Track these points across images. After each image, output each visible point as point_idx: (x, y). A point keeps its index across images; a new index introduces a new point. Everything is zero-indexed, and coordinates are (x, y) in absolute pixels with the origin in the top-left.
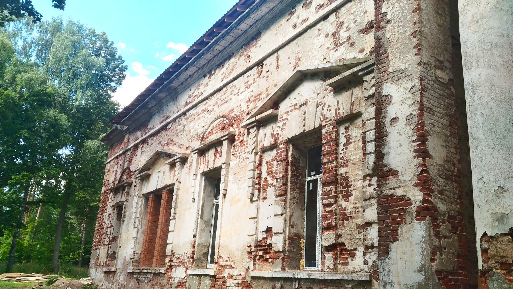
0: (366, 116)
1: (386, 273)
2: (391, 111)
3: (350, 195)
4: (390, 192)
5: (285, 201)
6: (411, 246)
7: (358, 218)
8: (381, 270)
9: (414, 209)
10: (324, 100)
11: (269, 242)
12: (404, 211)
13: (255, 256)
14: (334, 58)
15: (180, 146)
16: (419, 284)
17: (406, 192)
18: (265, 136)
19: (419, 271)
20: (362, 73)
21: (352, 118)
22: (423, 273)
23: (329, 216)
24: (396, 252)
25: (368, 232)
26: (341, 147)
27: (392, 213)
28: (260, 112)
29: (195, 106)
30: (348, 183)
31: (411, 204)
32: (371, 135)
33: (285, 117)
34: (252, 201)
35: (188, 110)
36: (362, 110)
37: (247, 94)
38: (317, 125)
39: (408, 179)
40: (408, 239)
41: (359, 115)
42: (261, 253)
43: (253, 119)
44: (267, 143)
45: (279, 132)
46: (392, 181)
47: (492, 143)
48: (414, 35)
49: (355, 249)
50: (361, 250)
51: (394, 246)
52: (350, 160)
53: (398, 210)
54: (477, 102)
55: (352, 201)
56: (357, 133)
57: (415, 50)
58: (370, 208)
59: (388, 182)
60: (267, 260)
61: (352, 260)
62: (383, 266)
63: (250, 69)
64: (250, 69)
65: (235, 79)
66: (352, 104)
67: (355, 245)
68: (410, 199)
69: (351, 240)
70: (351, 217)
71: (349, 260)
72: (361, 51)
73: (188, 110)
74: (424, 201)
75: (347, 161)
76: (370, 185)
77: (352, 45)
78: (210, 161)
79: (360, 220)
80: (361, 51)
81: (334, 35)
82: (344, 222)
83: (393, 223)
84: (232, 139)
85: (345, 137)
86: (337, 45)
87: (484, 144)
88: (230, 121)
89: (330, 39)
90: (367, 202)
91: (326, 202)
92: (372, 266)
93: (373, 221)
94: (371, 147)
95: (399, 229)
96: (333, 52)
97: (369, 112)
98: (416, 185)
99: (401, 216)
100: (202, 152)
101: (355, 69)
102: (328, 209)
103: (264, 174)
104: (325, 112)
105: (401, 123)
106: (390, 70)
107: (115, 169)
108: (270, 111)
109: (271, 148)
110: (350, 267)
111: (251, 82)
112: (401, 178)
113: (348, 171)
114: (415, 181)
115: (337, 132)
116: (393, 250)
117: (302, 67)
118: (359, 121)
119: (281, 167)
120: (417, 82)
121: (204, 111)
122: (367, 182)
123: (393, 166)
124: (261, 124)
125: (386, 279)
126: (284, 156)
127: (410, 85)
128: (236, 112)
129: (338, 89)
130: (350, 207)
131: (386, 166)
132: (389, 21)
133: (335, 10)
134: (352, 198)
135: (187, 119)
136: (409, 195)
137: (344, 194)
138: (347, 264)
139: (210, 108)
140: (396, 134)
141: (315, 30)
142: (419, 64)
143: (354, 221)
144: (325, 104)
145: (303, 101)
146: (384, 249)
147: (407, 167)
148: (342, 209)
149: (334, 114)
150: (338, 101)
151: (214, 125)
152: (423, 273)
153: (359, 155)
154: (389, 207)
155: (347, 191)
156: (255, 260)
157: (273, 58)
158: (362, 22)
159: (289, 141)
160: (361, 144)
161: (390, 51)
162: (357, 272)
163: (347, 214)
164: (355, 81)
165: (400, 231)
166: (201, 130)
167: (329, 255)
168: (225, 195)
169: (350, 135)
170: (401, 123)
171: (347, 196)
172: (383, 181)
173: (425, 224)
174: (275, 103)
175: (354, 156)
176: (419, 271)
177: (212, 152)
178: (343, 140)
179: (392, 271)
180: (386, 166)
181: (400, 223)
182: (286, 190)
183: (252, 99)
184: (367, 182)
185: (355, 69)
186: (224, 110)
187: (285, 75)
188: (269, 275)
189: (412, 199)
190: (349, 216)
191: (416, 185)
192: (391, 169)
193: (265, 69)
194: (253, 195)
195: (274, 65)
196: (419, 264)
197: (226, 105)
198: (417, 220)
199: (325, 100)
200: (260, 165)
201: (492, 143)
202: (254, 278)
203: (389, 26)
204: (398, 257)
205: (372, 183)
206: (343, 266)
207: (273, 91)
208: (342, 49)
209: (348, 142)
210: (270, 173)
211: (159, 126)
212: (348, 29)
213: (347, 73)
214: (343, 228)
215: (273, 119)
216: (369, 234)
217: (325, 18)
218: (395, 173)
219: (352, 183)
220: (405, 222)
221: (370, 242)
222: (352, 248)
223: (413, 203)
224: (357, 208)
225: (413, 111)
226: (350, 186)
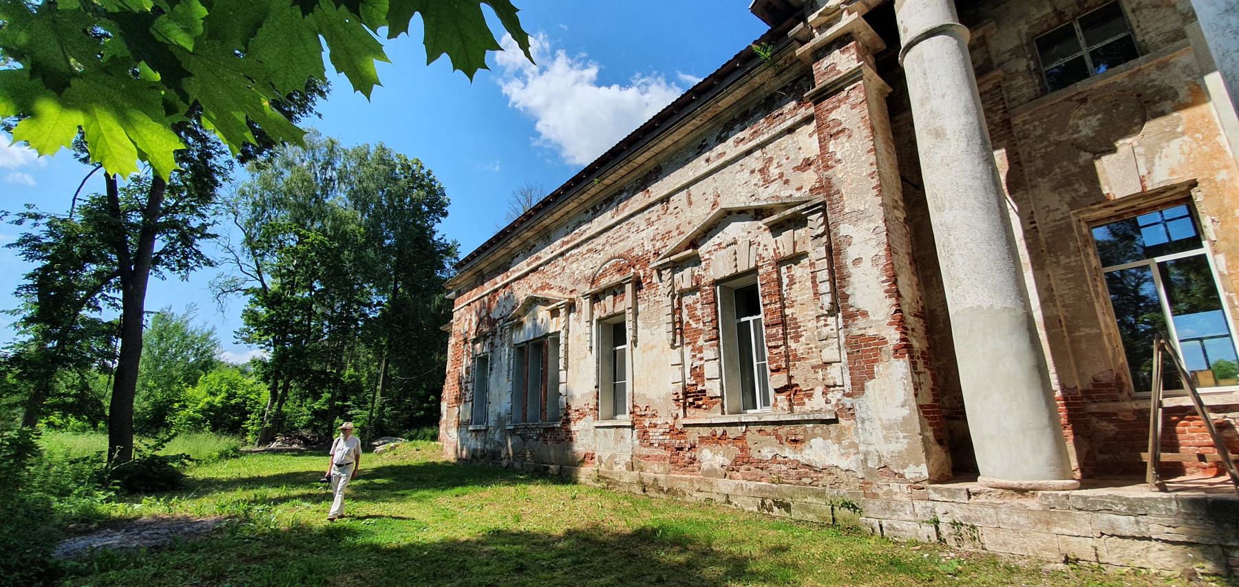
0: (813, 256)
2: (851, 253)
5: (718, 345)
11: (700, 388)
13: (684, 404)
14: (765, 196)
15: (562, 290)
16: (904, 418)
18: (684, 279)
21: (796, 258)
26: (784, 287)
27: (862, 356)
28: (674, 252)
29: (577, 246)
32: (824, 275)
33: (707, 256)
34: (673, 347)
35: (568, 250)
36: (809, 249)
37: (651, 231)
38: (752, 265)
41: (804, 255)
42: (691, 400)
43: (667, 260)
44: (686, 285)
45: (702, 273)
46: (861, 322)
48: (872, 175)
50: (819, 390)
51: (869, 384)
54: (954, 243)
57: (875, 192)
60: (699, 407)
63: (652, 205)
64: (652, 205)
65: (632, 215)
66: (795, 244)
71: (806, 400)
72: (799, 189)
73: (568, 250)
74: (902, 340)
76: (826, 325)
77: (787, 182)
78: (608, 305)
80: (799, 189)
81: (761, 171)
84: (638, 284)
86: (767, 182)
88: (628, 261)
89: (758, 176)
91: (773, 344)
92: (837, 405)
94: (825, 287)
96: (761, 189)
97: (818, 252)
98: (891, 324)
99: (875, 355)
100: (596, 298)
101: (798, 208)
102: (775, 351)
103: (685, 318)
104: (760, 251)
105: (866, 264)
106: (847, 210)
107: (468, 317)
108: (690, 251)
109: (693, 291)
110: (807, 408)
111: (654, 218)
112: (871, 317)
115: (779, 272)
117: (725, 203)
118: (805, 261)
119: (708, 310)
120: (881, 223)
121: (589, 251)
122: (822, 323)
124: (677, 266)
125: (864, 416)
126: (711, 298)
127: (872, 226)
128: (638, 252)
129: (776, 229)
132: (839, 161)
133: (761, 146)
135: (566, 260)
136: (883, 334)
139: (599, 248)
141: (737, 166)
142: (882, 205)
145: (730, 240)
146: (858, 388)
149: (772, 254)
151: (607, 266)
153: (810, 293)
156: (685, 409)
157: (683, 194)
158: (796, 159)
159: (716, 283)
160: (809, 284)
161: (843, 191)
164: (798, 221)
166: (588, 272)
167: (781, 397)
168: (635, 342)
171: (797, 337)
174: (694, 243)
175: (803, 294)
177: (610, 298)
178: (785, 281)
182: (718, 333)
183: (659, 237)
184: (822, 323)
185: (798, 208)
186: (621, 248)
187: (700, 214)
188: (708, 421)
191: (891, 324)
193: (672, 205)
194: (674, 341)
195: (685, 201)
197: (621, 244)
199: (759, 239)
200: (680, 308)
202: (685, 425)
203: (839, 166)
207: (689, 231)
208: (773, 188)
209: (792, 282)
210: (692, 316)
211: (527, 269)
212: (779, 166)
213: (789, 212)
215: (695, 261)
217: (748, 153)
218: (864, 314)
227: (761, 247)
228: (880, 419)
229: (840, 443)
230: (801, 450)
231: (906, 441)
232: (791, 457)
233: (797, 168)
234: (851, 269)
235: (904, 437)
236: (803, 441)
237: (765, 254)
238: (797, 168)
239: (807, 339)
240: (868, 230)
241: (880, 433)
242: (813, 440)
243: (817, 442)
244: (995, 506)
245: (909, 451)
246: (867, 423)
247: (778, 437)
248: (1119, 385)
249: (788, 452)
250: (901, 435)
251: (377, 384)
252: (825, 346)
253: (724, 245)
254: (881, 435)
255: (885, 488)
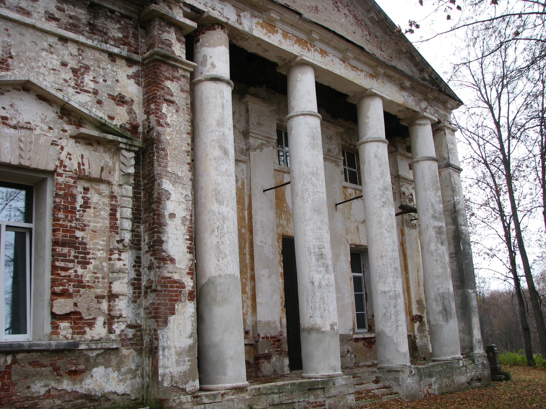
1: (165, 339)
3: (89, 263)
4: (169, 275)
6: (184, 319)
7: (98, 288)
8: (161, 338)
9: (187, 292)
10: (60, 141)
12: (180, 292)
16: (190, 346)
17: (181, 277)
19: (190, 337)
20: (124, 147)
22: (192, 338)
23: (65, 281)
24: (174, 323)
25: (116, 303)
30: (85, 249)
31: (184, 287)
38: (51, 168)
39: (183, 267)
40: (183, 314)
47: (234, 260)
49: (94, 319)
50: (100, 320)
52: (89, 226)
53: (175, 291)
54: (226, 229)
55: (91, 269)
56: (99, 200)
58: (119, 281)
59: (166, 266)
61: (90, 329)
62: (162, 335)
67: (93, 314)
68: (184, 284)
69: (88, 309)
70: (88, 286)
71: (87, 329)
75: (85, 225)
76: (119, 259)
79: (100, 290)
82: (79, 290)
83: (171, 300)
85: (83, 198)
87: (229, 258)
90: (115, 274)
92: (120, 335)
93: (121, 293)
95: (176, 305)
105: (178, 221)
112: (177, 265)
113: (85, 236)
114: (187, 271)
116: (171, 321)
123: (171, 254)
125: (165, 344)
130: (89, 275)
131: (165, 252)
134: (90, 267)
137: (80, 260)
138: (84, 333)
140: (173, 227)
143: (92, 290)
144: (62, 148)
147: (182, 258)
148: (77, 276)
149: (76, 166)
150: (82, 155)
152: (192, 338)
154: (167, 287)
155: (85, 258)
162: (96, 341)
163: (84, 282)
165: (176, 307)
169: (89, 199)
170: (178, 221)
172: (162, 264)
173: (194, 304)
176: (190, 337)
179: (170, 338)
180: (165, 252)
181: (176, 300)
189: (186, 284)
190: (87, 284)
192: (169, 256)
196: (190, 332)
198: (189, 300)
201: (234, 260)
204: (175, 327)
205: (122, 257)
206: (79, 336)
209: (86, 205)
214: (79, 296)
216: (118, 305)
218: (172, 260)
219: (91, 251)
220: (181, 301)
221: (118, 313)
222: (91, 317)
223: (186, 287)
224: (98, 278)
225: (187, 215)
226: (88, 253)
227: (64, 153)
228: (175, 347)
229: (119, 370)
230: (81, 381)
231: (189, 363)
232: (69, 389)
233: (113, 98)
234: (168, 221)
235: (189, 361)
236: (83, 371)
237: (67, 162)
238: (113, 98)
239: (95, 267)
240: (182, 194)
241: (174, 358)
242: (95, 370)
243: (98, 371)
244: (232, 400)
245: (191, 370)
246: (166, 350)
247: (56, 369)
248: (487, 344)
249: (66, 385)
250: (187, 359)
251: (245, 243)
252: (116, 279)
253: (13, 122)
254: (174, 360)
255: (177, 401)
